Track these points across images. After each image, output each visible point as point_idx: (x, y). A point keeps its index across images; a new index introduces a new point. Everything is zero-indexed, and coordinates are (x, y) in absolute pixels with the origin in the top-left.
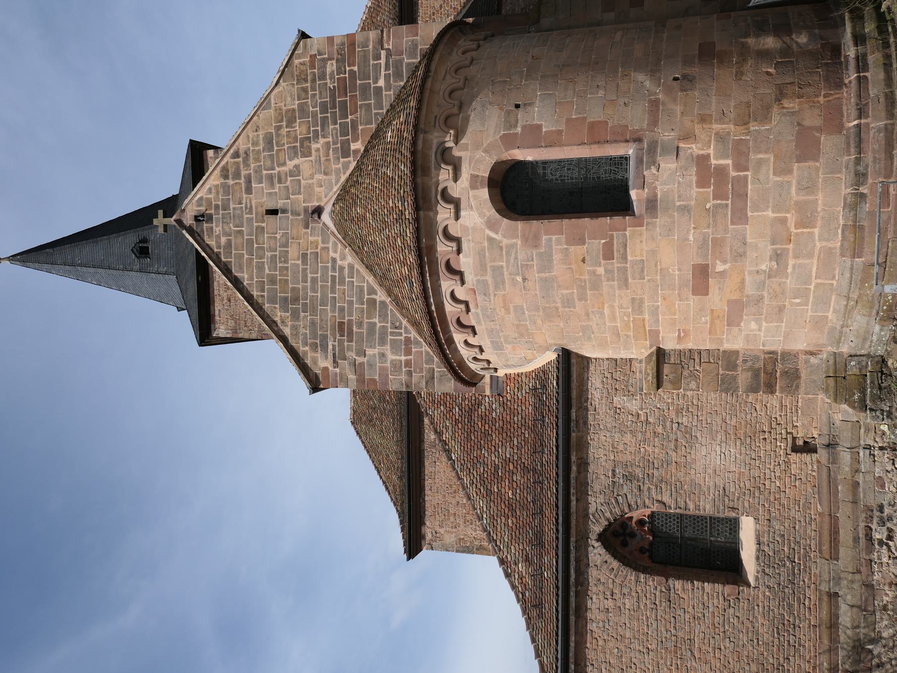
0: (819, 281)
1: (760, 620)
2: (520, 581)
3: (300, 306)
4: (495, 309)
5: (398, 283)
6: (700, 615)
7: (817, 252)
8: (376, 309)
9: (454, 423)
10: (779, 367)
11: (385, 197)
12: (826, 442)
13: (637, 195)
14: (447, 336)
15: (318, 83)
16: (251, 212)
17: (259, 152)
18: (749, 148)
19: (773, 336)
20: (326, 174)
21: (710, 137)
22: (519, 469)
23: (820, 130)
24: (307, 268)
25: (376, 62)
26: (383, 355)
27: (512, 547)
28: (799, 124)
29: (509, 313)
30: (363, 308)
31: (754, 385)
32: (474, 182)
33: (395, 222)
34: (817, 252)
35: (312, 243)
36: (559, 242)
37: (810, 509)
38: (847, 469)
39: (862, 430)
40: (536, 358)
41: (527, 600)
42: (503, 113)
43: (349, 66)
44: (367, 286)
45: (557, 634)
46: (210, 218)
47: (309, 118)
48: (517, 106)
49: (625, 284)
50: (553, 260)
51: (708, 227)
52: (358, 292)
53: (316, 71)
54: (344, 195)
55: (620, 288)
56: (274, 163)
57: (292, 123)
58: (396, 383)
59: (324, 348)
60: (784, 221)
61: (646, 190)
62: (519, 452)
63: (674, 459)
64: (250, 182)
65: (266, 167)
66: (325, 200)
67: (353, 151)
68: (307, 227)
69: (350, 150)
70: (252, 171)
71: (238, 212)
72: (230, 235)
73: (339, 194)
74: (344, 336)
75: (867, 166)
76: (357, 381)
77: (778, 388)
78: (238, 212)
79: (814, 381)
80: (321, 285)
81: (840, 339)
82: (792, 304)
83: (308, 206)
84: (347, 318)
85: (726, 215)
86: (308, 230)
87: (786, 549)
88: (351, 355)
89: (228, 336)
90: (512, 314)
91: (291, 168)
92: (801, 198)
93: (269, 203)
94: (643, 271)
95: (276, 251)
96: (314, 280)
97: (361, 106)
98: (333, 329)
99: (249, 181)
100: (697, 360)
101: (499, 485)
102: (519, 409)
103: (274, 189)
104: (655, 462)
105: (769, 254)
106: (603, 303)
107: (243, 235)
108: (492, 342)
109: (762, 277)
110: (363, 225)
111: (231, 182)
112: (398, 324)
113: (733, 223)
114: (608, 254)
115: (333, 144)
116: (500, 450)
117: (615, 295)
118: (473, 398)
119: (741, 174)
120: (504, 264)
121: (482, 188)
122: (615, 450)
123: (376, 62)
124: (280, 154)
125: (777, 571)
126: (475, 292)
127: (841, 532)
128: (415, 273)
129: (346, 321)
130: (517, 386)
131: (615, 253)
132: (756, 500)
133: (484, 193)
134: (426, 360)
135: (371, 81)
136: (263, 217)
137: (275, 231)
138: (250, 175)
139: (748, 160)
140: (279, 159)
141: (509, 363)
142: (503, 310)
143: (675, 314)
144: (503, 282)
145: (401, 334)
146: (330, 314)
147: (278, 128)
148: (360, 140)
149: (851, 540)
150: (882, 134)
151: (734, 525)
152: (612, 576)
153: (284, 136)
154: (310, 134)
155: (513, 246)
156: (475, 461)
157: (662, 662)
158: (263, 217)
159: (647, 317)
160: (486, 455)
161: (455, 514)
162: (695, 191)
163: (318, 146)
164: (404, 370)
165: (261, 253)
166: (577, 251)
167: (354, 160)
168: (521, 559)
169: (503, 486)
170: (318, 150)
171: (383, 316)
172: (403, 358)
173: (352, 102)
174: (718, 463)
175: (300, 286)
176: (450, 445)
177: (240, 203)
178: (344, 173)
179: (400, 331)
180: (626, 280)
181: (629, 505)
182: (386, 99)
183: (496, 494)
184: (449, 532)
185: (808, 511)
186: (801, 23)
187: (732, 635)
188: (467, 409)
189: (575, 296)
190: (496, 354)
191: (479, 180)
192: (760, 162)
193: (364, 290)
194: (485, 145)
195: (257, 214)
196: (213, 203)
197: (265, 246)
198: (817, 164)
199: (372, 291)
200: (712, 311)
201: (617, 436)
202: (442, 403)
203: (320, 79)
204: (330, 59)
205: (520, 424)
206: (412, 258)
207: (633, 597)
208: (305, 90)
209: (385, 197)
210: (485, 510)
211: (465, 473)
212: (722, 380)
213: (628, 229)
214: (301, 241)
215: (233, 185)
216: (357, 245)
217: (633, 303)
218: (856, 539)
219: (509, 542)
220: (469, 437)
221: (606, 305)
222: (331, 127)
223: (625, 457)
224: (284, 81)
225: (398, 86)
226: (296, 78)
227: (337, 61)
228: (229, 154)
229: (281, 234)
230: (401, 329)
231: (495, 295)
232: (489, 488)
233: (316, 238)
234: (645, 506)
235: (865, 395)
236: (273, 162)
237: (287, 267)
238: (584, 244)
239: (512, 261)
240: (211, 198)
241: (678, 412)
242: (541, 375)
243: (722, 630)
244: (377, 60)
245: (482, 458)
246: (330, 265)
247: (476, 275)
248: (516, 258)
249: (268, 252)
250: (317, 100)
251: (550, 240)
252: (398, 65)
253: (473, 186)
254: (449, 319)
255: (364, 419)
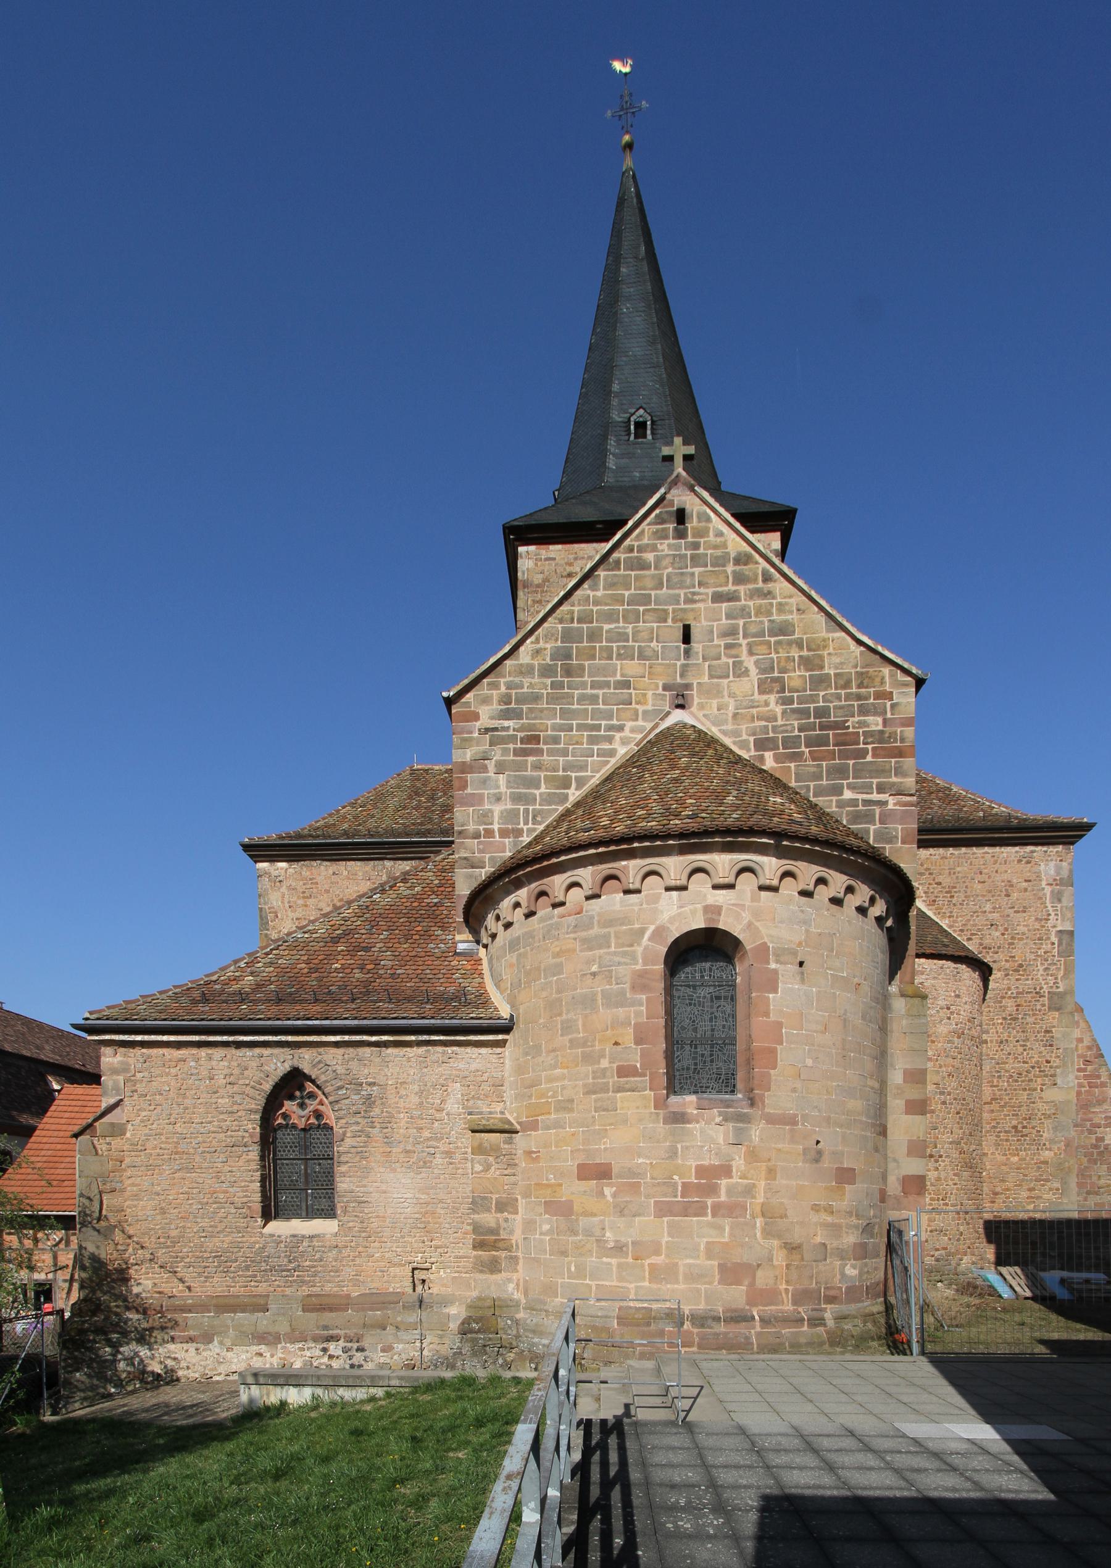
0: (594, 1288)
1: (228, 1239)
2: (232, 978)
3: (559, 679)
4: (558, 940)
5: (589, 814)
6: (223, 1178)
7: (624, 1284)
8: (558, 788)
9: (418, 897)
10: (503, 1254)
11: (699, 794)
12: (426, 1300)
13: (691, 1102)
14: (524, 879)
15: (856, 703)
16: (688, 601)
17: (769, 613)
18: (737, 1217)
19: (534, 1247)
20: (735, 715)
21: (751, 1179)
22: (367, 976)
23: (752, 1284)
24: (610, 689)
25: (874, 786)
26: (498, 799)
27: (272, 969)
28: (759, 1266)
29: (553, 958)
30: (558, 771)
31: (481, 1230)
32: (713, 910)
33: (665, 807)
34: (624, 1284)
35: (645, 695)
36: (638, 1014)
37: (354, 1285)
38: (399, 1319)
39: (440, 1333)
40: (501, 993)
41: (210, 986)
42: (794, 946)
43: (873, 748)
44: (587, 776)
45: (174, 1020)
46: (681, 534)
47: (810, 690)
48: (801, 964)
49: (589, 1091)
50: (617, 1008)
51: (652, 1178)
52: (580, 763)
53: (872, 701)
54: (706, 741)
55: (585, 1085)
56: (753, 637)
57: (805, 665)
58: (464, 817)
59: (506, 715)
60: (657, 1252)
61: (695, 1112)
62: (388, 976)
63: (394, 1150)
64: (729, 600)
65: (747, 626)
66: (700, 714)
67: (762, 756)
68: (666, 688)
69: (764, 751)
70: (743, 602)
71: (688, 580)
72: (656, 568)
73: (707, 734)
74: (521, 743)
75: (711, 1328)
76: (464, 763)
77: (480, 1253)
78: (688, 580)
79: (489, 1287)
80: (588, 709)
81: (534, 1310)
82: (569, 1264)
83: (693, 690)
84: (545, 747)
85: (665, 1195)
86: (661, 688)
87: (308, 1263)
88: (497, 755)
89: (519, 574)
90: (552, 961)
91: (745, 664)
92: (681, 1269)
93: (699, 630)
94: (604, 1110)
95: (634, 641)
96: (594, 699)
97: (820, 766)
98: (531, 728)
99: (732, 597)
100: (506, 1172)
101: (346, 953)
102: (441, 976)
103: (718, 637)
104: (389, 1130)
105: (623, 1239)
106: (567, 1067)
107: (657, 589)
108: (518, 938)
109: (598, 1233)
110: (665, 765)
111: (730, 568)
112: (539, 819)
113: (655, 1202)
114: (624, 1071)
115: (773, 727)
116: (389, 953)
117: (576, 1080)
118: (451, 921)
119: (709, 1211)
120: (613, 949)
121: (705, 920)
122: (398, 1085)
123: (874, 786)
124: (765, 647)
125: (283, 1255)
126: (578, 913)
127: (333, 1315)
128: (601, 833)
129: (541, 746)
130: (468, 972)
131: (625, 1079)
132: (358, 1234)
133: (699, 923)
134: (494, 857)
135: (851, 780)
136: (681, 620)
137: (661, 639)
138: (738, 599)
139: (723, 1216)
140: (757, 645)
141: (494, 961)
142: (558, 949)
143: (556, 1146)
144: (590, 949)
145: (526, 823)
146: (549, 723)
147: (799, 644)
148: (776, 765)
149: (325, 1323)
150: (743, 1340)
151: (329, 1213)
152: (252, 1083)
153: (788, 653)
154: (789, 692)
155: (634, 960)
156: (373, 923)
157: (163, 1138)
158: (681, 620)
159: (553, 1116)
160: (382, 937)
161: (306, 906)
162: (693, 1164)
163: (772, 705)
164: (481, 828)
165: (632, 617)
166: (628, 1037)
167: (750, 756)
168: (259, 979)
169: (345, 957)
170: (767, 704)
171: (548, 799)
172: (496, 827)
173: (826, 754)
174: (395, 1196)
175: (586, 678)
176: (391, 892)
177: (700, 584)
178: (734, 743)
179: (530, 822)
180: (595, 1093)
181: (337, 1102)
182: (828, 801)
183: (334, 949)
184: (283, 897)
185: (350, 1284)
186: (866, 1270)
187: (206, 1212)
188: (438, 912)
189: (575, 1035)
190: (505, 944)
191: (714, 916)
192: (721, 1229)
193: (581, 772)
194: (757, 924)
195: (684, 610)
196: (702, 540)
197: (641, 624)
198: (716, 1283)
199: (581, 782)
200: (561, 1185)
201: (416, 1088)
202: (443, 882)
203: (860, 706)
204: (885, 722)
205: (422, 976)
206: (620, 828)
207: (232, 1107)
208: (847, 685)
209: (699, 794)
210: (314, 936)
211: (356, 911)
212: (485, 1198)
213: (652, 1093)
214: (646, 679)
215: (725, 571)
216: (640, 760)
217: (568, 1101)
218: (326, 1328)
219: (277, 965)
220: (401, 915)
221: (565, 1071)
222: (796, 723)
223: (391, 1097)
224: (861, 653)
225: (841, 818)
226: (864, 670)
227: (881, 732)
228: (768, 567)
229: (656, 649)
230: (533, 824)
231: (575, 939)
232: (341, 940)
233: (650, 702)
234: (338, 1119)
235: (476, 1333)
236: (754, 636)
237: (612, 659)
238: (637, 1043)
239: (617, 959)
240: (708, 537)
241: (449, 1154)
242: (483, 1000)
243: (210, 1201)
244: (878, 789)
245: (377, 932)
246: (615, 722)
247: (599, 914)
248: (619, 964)
249: (633, 628)
250: (832, 702)
251: (641, 1005)
252: (869, 818)
253: (707, 909)
254: (545, 881)
255: (418, 784)
